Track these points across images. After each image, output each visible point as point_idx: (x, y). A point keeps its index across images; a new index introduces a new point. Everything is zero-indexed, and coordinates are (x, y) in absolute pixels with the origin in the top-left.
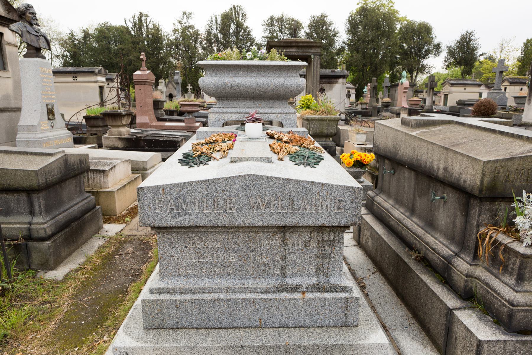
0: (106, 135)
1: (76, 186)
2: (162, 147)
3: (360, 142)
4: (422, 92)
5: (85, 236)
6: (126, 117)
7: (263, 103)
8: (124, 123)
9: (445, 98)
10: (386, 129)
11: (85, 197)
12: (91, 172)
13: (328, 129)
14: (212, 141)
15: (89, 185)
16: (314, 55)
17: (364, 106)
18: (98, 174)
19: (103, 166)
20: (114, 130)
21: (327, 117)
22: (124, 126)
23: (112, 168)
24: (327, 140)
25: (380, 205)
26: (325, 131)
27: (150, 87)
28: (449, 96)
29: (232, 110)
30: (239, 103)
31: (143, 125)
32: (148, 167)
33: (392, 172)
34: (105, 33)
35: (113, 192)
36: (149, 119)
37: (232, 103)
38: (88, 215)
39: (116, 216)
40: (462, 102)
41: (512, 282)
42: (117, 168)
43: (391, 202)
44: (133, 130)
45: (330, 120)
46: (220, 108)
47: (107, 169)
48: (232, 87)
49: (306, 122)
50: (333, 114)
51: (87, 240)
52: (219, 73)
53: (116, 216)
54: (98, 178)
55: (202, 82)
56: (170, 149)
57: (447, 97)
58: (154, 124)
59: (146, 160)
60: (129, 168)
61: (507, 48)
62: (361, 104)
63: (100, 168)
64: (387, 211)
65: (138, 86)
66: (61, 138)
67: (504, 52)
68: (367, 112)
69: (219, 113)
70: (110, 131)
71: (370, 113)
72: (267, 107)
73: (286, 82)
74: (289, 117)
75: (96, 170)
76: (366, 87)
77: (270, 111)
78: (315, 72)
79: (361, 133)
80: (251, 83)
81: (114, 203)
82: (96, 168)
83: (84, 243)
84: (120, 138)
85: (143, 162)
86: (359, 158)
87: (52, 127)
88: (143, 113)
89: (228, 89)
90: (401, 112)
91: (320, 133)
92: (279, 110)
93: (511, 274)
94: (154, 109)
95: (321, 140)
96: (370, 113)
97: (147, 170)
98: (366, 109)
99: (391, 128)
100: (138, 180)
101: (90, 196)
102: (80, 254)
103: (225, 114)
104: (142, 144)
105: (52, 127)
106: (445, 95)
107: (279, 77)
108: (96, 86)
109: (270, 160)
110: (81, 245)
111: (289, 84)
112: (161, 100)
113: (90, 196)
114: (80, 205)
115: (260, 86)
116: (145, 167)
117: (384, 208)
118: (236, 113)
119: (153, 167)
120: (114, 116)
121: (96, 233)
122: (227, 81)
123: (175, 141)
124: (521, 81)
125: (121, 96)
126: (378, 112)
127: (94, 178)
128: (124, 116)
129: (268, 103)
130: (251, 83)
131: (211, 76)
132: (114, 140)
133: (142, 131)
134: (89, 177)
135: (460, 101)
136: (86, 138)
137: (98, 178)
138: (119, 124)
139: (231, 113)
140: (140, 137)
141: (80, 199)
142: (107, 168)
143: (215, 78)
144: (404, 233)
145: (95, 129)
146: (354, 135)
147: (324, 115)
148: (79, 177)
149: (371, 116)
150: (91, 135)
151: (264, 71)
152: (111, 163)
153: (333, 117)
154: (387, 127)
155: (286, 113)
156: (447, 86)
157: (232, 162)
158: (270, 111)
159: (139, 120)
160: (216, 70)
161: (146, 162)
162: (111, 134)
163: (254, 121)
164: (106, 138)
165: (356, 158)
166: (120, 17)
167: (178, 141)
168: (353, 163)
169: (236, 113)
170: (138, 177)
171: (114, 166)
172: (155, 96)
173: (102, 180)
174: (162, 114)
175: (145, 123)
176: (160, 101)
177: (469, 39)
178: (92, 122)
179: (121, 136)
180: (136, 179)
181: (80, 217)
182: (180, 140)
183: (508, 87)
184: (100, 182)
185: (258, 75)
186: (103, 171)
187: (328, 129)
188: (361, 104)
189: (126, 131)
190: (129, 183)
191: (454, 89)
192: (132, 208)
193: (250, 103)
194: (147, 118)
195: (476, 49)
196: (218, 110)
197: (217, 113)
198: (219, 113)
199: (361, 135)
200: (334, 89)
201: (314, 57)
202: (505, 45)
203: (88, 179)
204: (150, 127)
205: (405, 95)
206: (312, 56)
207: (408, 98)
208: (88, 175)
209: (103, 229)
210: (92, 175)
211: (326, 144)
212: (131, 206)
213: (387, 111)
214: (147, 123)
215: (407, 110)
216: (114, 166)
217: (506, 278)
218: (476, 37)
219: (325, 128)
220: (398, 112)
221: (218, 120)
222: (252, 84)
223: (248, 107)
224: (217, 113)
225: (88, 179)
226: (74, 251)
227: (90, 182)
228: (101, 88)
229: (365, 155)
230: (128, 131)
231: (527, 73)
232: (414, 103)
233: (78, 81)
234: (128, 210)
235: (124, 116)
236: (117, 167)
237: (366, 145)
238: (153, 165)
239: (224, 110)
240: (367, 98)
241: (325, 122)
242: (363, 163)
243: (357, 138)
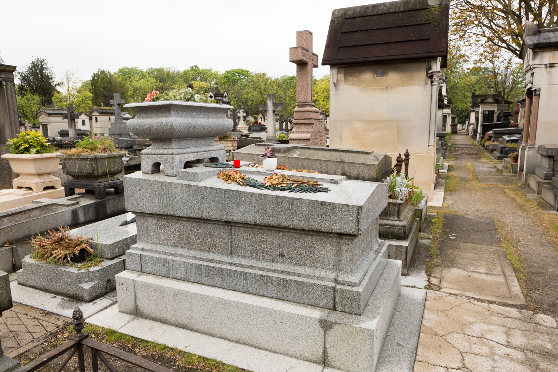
13: (114, 167)
16: (6, 81)
28: (48, 126)
34: (160, 70)
41: (396, 219)
57: (47, 128)
61: (73, 79)
67: (71, 83)
72: (200, 146)
78: (10, 102)
93: (393, 216)
124: (108, 111)
135: (62, 131)
156: (43, 115)
166: (244, 68)
177: (42, 66)
183: (98, 117)
187: (114, 167)
191: (52, 119)
195: (51, 79)
201: (6, 84)
202: (70, 76)
206: (4, 83)
217: (392, 218)
218: (49, 66)
231: (102, 104)
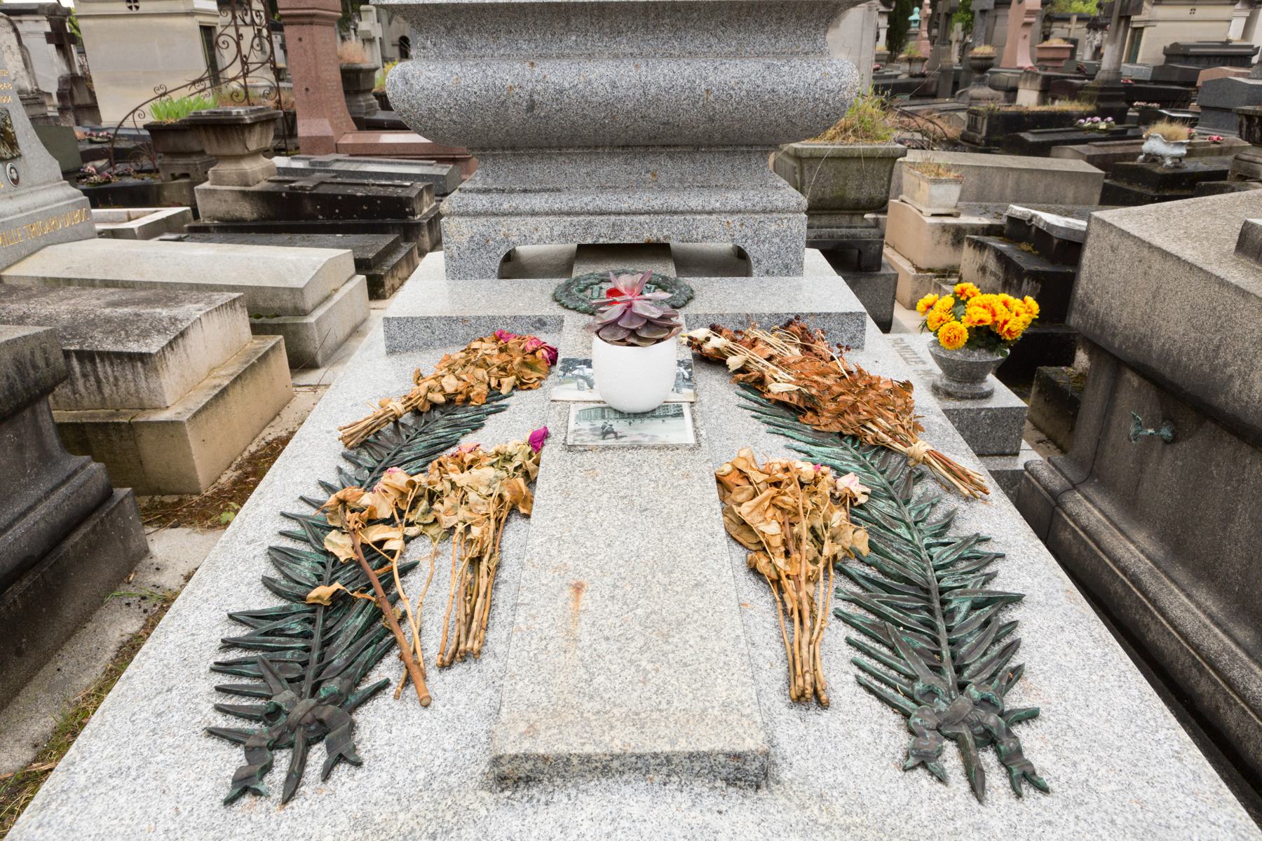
0: (206, 185)
1: (20, 448)
2: (363, 215)
3: (940, 206)
4: (1068, 20)
5: (69, 612)
6: (258, 129)
7: (667, 167)
8: (253, 144)
9: (1132, 37)
10: (1157, 263)
11: (63, 475)
12: (102, 360)
13: (860, 187)
14: (440, 398)
15: (103, 398)
17: (918, 68)
18: (128, 367)
19: (145, 334)
20: (226, 169)
21: (862, 146)
22: (254, 154)
23: (170, 344)
24: (857, 220)
25: (1098, 544)
26: (852, 194)
27: (329, 30)
28: (1145, 32)
29: (538, 202)
30: (569, 168)
31: (320, 144)
32: (309, 304)
33: (1166, 432)
35: (180, 423)
36: (332, 124)
37: (538, 170)
38: (76, 537)
39: (198, 494)
40: (1181, 51)
42: (194, 338)
43: (1141, 537)
44: (281, 161)
45: (870, 158)
46: (487, 191)
47: (154, 349)
48: (532, 107)
49: (791, 162)
50: (878, 138)
51: (84, 619)
52: (476, 41)
53: (198, 494)
54: (130, 377)
55: (400, 86)
56: (389, 220)
58: (349, 139)
59: (301, 285)
60: (242, 322)
62: (910, 60)
63: (133, 347)
64: (1136, 581)
65: (294, 28)
66: (47, 215)
68: (926, 86)
69: (486, 214)
70: (214, 172)
71: (933, 89)
72: (682, 185)
73: (771, 80)
74: (773, 228)
75: (119, 355)
76: (916, 9)
77: (695, 202)
79: (946, 181)
80: (614, 86)
81: (188, 456)
82: (119, 348)
83: (68, 638)
84: (244, 194)
85: (291, 289)
86: (988, 319)
87: (16, 182)
88: (316, 109)
89: (515, 116)
90: (1021, 86)
91: (834, 199)
92: (734, 199)
94: (347, 93)
95: (988, 460)
96: (933, 89)
97: (305, 313)
98: (923, 75)
99: (1192, 266)
100: (272, 357)
101: (83, 467)
102: (49, 690)
103: (509, 220)
104: (309, 207)
105: (16, 182)
106: (1135, 29)
107: (736, 54)
108: (193, 24)
109: (753, 767)
110: (58, 647)
111: (781, 89)
112: (365, 66)
113: (83, 467)
114: (42, 510)
115: (657, 100)
116: (300, 305)
117: (1116, 561)
118: (554, 213)
119: (327, 298)
120: (221, 128)
121: (120, 581)
122: (509, 80)
123: (399, 199)
125: (252, 59)
126: (956, 85)
127: (116, 379)
128: (252, 126)
129: (687, 166)
130: (614, 86)
131: (440, 56)
132: (230, 198)
133: (312, 164)
134: (101, 375)
135: (1175, 46)
136: (159, 187)
137: (130, 377)
138: (239, 150)
139: (534, 214)
140: (301, 188)
141: (44, 486)
142: (154, 345)
143: (456, 68)
144: (1204, 687)
145: (181, 161)
146: (924, 185)
147: (852, 139)
148: (27, 413)
149: (934, 96)
150: (174, 177)
151: (675, 29)
152: (174, 320)
153: (880, 146)
154: (1166, 255)
155: (764, 211)
157: (502, 780)
158: (695, 202)
159: (304, 129)
160: (459, 30)
161: (301, 291)
162: (219, 180)
163: (633, 333)
164: (207, 191)
165: (976, 318)
167: (409, 199)
168: (966, 336)
169: (554, 213)
170: (273, 348)
171: (182, 334)
172: (346, 56)
173: (143, 384)
174: (371, 106)
175: (321, 138)
176: (360, 71)
178: (172, 141)
179: (247, 185)
180: (264, 358)
181: (45, 554)
182: (414, 194)
184: (137, 392)
185: (647, 49)
186: (142, 358)
187: (860, 187)
188: (910, 60)
189: (262, 169)
190: (238, 379)
192: (253, 456)
193: (613, 168)
194: (326, 122)
196: (482, 202)
197: (477, 214)
198: (486, 214)
199: (946, 186)
200: (842, 25)
203: (98, 381)
204: (337, 149)
205: (1027, 32)
207: (1032, 46)
208: (95, 370)
209: (147, 561)
210: (109, 370)
211: (853, 236)
212: (253, 448)
213: (981, 82)
214: (327, 137)
215: (1039, 80)
216: (182, 334)
219: (852, 184)
220: (1011, 84)
221: (481, 244)
222: (621, 93)
223: (602, 188)
224: (477, 214)
225: (98, 381)
226: (30, 679)
227: (107, 391)
228: (207, 30)
229: (1006, 304)
230: (268, 170)
232: (1050, 55)
233: (141, 11)
234: (239, 467)
235: (252, 126)
236: (192, 334)
237: (957, 215)
238: (326, 293)
239: (507, 203)
240: (919, 45)
241: (854, 166)
242: (998, 337)
243: (931, 197)
